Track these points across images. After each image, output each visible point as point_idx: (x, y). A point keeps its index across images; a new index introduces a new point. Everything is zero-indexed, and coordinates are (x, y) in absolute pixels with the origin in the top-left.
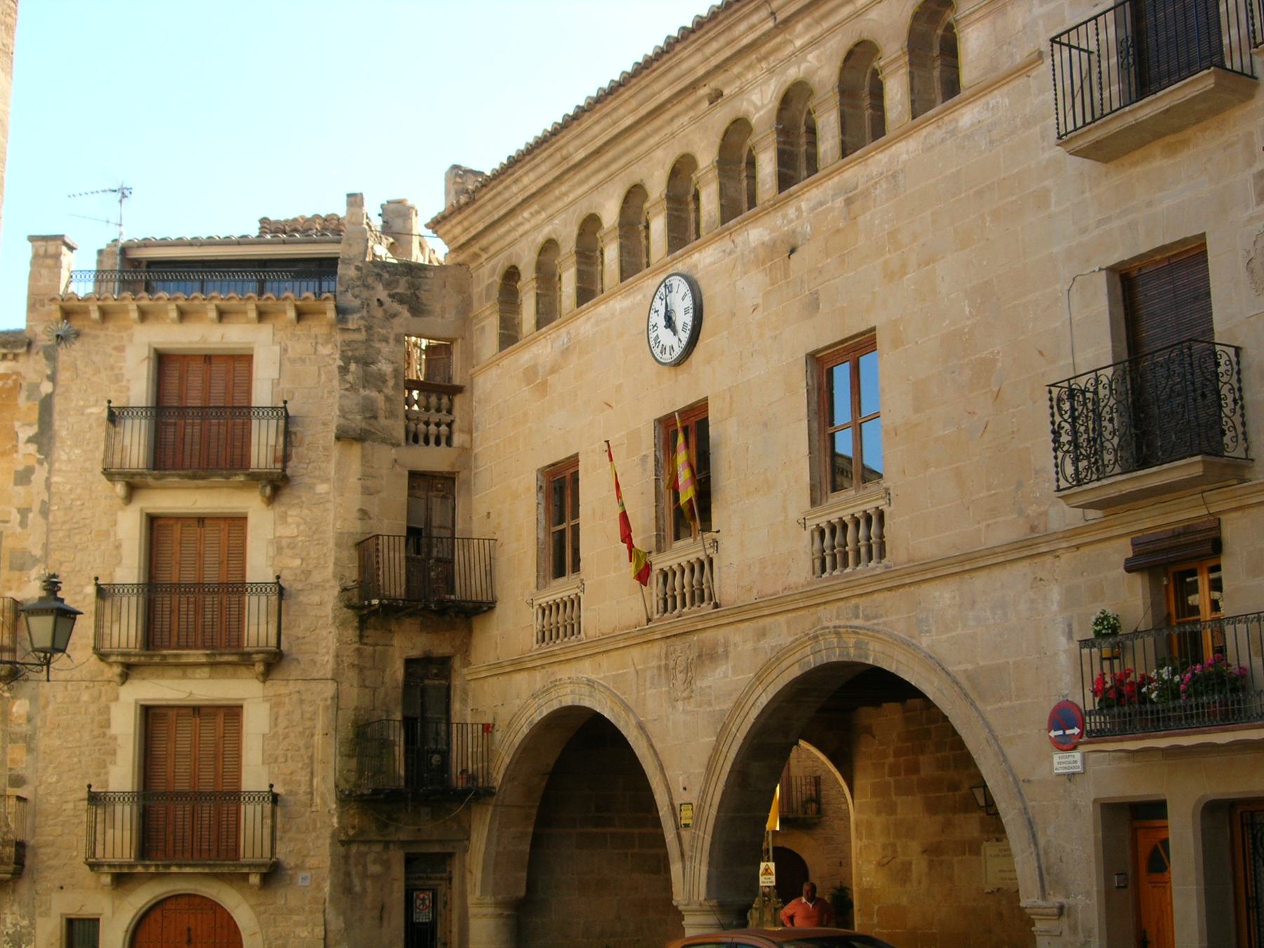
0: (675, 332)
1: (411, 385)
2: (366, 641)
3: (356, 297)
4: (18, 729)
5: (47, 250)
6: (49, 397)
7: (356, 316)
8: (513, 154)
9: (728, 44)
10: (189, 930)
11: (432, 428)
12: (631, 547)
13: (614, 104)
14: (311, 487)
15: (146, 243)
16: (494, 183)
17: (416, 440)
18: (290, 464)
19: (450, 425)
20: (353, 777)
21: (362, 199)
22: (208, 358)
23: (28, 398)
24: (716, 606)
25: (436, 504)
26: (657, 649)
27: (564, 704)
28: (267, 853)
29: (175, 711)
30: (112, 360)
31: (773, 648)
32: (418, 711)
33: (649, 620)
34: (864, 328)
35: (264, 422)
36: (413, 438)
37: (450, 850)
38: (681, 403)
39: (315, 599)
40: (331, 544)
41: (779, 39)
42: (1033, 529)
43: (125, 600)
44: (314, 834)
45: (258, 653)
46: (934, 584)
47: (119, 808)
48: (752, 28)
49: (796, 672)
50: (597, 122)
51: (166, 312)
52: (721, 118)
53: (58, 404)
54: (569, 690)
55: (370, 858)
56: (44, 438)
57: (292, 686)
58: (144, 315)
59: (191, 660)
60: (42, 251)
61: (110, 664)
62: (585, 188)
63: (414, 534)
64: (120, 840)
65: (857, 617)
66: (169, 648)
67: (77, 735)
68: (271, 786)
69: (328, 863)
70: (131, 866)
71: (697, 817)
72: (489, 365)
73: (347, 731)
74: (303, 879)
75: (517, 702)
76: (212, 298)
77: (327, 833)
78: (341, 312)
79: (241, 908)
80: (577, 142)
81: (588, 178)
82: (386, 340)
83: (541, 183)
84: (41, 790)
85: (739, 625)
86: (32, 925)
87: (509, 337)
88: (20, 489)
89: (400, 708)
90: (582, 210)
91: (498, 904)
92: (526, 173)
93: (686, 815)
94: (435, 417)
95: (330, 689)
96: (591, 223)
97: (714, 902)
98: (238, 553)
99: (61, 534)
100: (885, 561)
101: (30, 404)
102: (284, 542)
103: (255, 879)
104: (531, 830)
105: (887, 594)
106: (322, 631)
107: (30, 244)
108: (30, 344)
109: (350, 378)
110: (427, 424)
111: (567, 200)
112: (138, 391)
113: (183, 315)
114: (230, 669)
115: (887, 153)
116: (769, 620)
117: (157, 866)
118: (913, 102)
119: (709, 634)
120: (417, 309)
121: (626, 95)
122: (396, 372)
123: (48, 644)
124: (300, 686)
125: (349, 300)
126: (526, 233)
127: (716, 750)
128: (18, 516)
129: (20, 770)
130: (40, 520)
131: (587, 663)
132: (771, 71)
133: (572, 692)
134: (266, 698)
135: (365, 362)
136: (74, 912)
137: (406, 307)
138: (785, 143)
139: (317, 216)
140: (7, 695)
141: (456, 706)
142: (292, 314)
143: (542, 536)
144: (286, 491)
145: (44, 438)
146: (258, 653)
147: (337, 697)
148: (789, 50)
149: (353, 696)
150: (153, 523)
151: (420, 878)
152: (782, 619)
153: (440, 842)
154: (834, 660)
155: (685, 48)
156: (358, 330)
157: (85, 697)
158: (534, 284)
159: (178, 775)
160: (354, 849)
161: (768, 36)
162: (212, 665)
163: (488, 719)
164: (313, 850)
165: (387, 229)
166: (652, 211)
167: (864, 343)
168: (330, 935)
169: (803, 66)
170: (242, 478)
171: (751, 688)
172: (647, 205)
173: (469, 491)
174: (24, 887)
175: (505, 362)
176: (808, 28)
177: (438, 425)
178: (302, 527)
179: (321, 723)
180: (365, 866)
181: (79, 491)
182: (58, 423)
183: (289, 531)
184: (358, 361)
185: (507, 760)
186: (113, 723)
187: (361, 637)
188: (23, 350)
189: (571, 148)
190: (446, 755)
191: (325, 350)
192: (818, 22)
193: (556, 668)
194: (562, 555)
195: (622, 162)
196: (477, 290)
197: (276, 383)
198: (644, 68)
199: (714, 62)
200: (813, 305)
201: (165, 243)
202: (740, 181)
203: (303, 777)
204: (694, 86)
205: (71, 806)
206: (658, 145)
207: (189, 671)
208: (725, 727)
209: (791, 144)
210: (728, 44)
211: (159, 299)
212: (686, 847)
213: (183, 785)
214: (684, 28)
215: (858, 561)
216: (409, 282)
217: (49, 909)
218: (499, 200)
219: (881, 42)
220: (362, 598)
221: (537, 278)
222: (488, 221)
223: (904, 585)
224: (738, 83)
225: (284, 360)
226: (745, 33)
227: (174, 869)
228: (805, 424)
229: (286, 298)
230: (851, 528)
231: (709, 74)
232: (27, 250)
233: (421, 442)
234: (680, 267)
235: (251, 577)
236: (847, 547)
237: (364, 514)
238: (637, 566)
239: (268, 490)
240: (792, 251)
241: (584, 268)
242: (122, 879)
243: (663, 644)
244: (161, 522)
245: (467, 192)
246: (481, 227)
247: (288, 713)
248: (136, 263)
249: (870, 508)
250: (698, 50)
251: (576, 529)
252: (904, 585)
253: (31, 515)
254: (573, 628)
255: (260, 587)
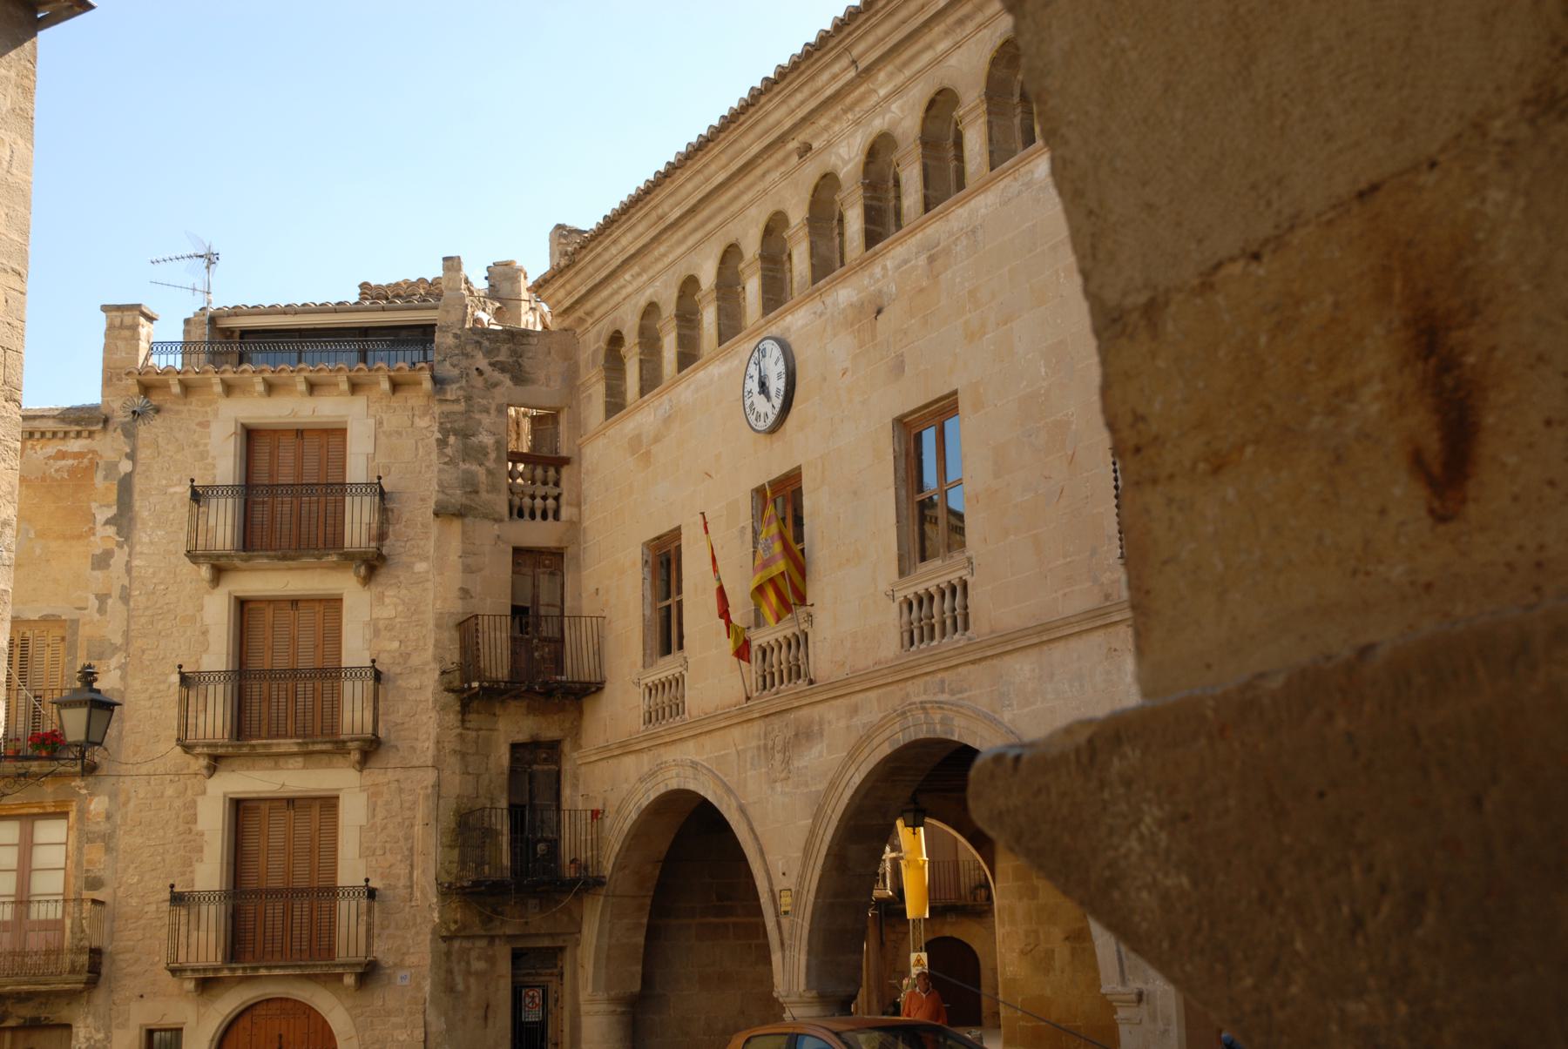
0: (768, 398)
1: (516, 457)
2: (468, 725)
3: (454, 366)
4: (96, 828)
5: (124, 320)
6: (129, 475)
7: (454, 386)
8: (609, 213)
9: (812, 95)
10: (280, 1036)
11: (538, 501)
12: (728, 622)
13: (688, 174)
14: (410, 566)
15: (237, 311)
16: (593, 244)
17: (521, 515)
18: (387, 542)
19: (557, 498)
20: (455, 868)
21: (460, 263)
22: (300, 433)
23: (106, 477)
24: (811, 682)
25: (544, 582)
26: (757, 728)
27: (670, 788)
28: (362, 952)
29: (268, 804)
30: (196, 437)
31: (864, 726)
32: (527, 797)
33: (748, 698)
34: (946, 391)
35: (357, 499)
36: (517, 512)
37: (560, 944)
38: (777, 472)
39: (415, 683)
40: (431, 625)
41: (862, 89)
42: (1107, 597)
43: (211, 688)
44: (413, 931)
45: (352, 740)
46: (1016, 655)
47: (204, 908)
48: (834, 77)
49: (886, 750)
50: (688, 180)
51: (253, 385)
52: (810, 172)
53: (139, 484)
54: (674, 773)
55: (474, 954)
56: (124, 519)
57: (391, 775)
58: (229, 389)
59: (282, 749)
60: (117, 322)
61: (197, 756)
62: (683, 248)
63: (518, 611)
64: (205, 941)
65: (943, 692)
66: (259, 737)
67: (161, 833)
68: (367, 880)
69: (429, 961)
70: (216, 970)
71: (796, 905)
72: (597, 434)
73: (449, 820)
74: (402, 978)
75: (626, 786)
76: (300, 370)
77: (430, 926)
78: (438, 382)
79: (335, 1010)
80: (671, 201)
81: (685, 237)
82: (487, 411)
83: (639, 244)
84: (120, 893)
85: (834, 702)
86: (108, 1038)
87: (615, 405)
88: (98, 573)
89: (505, 795)
90: (680, 272)
91: (611, 1000)
92: (624, 233)
93: (786, 902)
94: (540, 490)
95: (430, 777)
96: (690, 285)
97: (814, 993)
98: (334, 636)
99: (143, 620)
100: (968, 633)
101: (107, 483)
102: (381, 624)
103: (349, 980)
104: (645, 921)
105: (971, 667)
106: (421, 715)
107: (103, 315)
108: (106, 421)
109: (449, 451)
110: (533, 497)
111: (667, 261)
112: (225, 467)
113: (270, 388)
114: (325, 758)
115: (967, 207)
116: (861, 696)
117: (244, 969)
118: (991, 153)
119: (805, 712)
120: (520, 378)
121: (715, 151)
122: (499, 445)
123: (82, 737)
124: (399, 774)
125: (446, 370)
126: (629, 296)
127: (812, 833)
128: (96, 603)
129: (97, 871)
130: (120, 606)
131: (691, 744)
132: (857, 122)
133: (678, 775)
134: (363, 788)
135: (465, 435)
136: (153, 1021)
137: (508, 376)
138: (872, 198)
139: (422, 280)
140: (84, 792)
141: (567, 792)
142: (385, 385)
143: (648, 612)
144: (383, 571)
145: (124, 519)
146: (352, 740)
147: (438, 785)
148: (874, 99)
149: (455, 783)
150: (243, 607)
151: (529, 974)
152: (872, 695)
153: (551, 935)
154: (921, 736)
155: (770, 100)
156: (457, 401)
157: (170, 792)
158: (637, 349)
159: (270, 870)
160: (456, 944)
161: (850, 86)
162: (307, 754)
163: (598, 806)
164: (413, 943)
165: (493, 293)
166: (747, 272)
167: (944, 409)
168: (430, 1037)
169: (887, 117)
170: (335, 558)
171: (844, 767)
172: (742, 266)
173: (578, 568)
174: (100, 997)
175: (611, 432)
176: (890, 76)
177: (544, 498)
178: (400, 608)
179: (421, 813)
180: (468, 963)
181: (162, 574)
182: (138, 503)
183: (387, 612)
184: (457, 435)
185: (617, 848)
186: (200, 818)
187: (463, 721)
188: (100, 426)
189: (666, 207)
190: (554, 845)
191: (422, 423)
192: (900, 69)
193: (662, 750)
194: (667, 633)
195: (718, 220)
196: (584, 356)
197: (370, 458)
198: (731, 120)
199: (800, 114)
200: (899, 367)
201: (256, 311)
202: (832, 239)
203: (402, 870)
204: (782, 139)
205: (153, 907)
206: (752, 202)
207: (282, 762)
208: (820, 808)
209: (879, 199)
210: (812, 95)
211: (244, 371)
212: (786, 935)
213: (276, 882)
214: (766, 79)
215: (943, 635)
216: (510, 350)
217: (128, 1020)
218: (599, 262)
219: (960, 91)
220: (462, 682)
221: (640, 343)
222: (590, 284)
223: (985, 658)
224: (826, 136)
225: (379, 433)
226: (828, 83)
227: (263, 972)
228: (892, 491)
229: (378, 369)
230: (937, 599)
231: (795, 127)
232: (101, 321)
233: (550, 518)
234: (774, 330)
235: (346, 662)
236: (934, 618)
237: (465, 593)
238: (736, 641)
239: (363, 570)
240: (879, 312)
241: (687, 332)
242: (207, 984)
243: (761, 722)
244: (251, 605)
245: (566, 254)
246: (583, 290)
247: (387, 803)
248: (228, 333)
249: (954, 577)
250: (783, 102)
251: (680, 604)
252: (985, 658)
253: (110, 601)
254: (677, 708)
255: (356, 672)
